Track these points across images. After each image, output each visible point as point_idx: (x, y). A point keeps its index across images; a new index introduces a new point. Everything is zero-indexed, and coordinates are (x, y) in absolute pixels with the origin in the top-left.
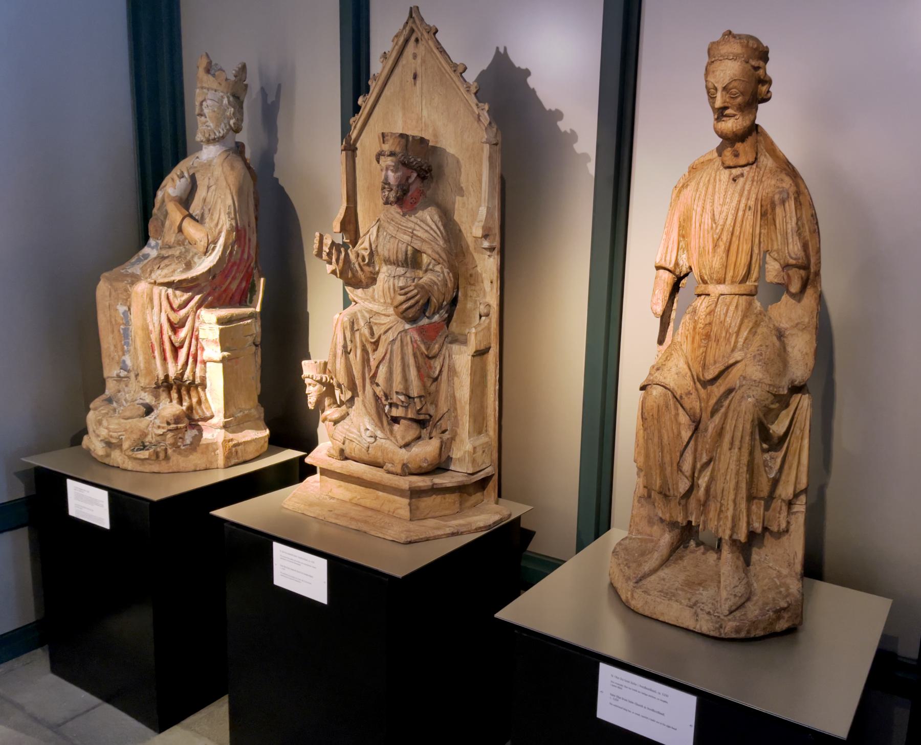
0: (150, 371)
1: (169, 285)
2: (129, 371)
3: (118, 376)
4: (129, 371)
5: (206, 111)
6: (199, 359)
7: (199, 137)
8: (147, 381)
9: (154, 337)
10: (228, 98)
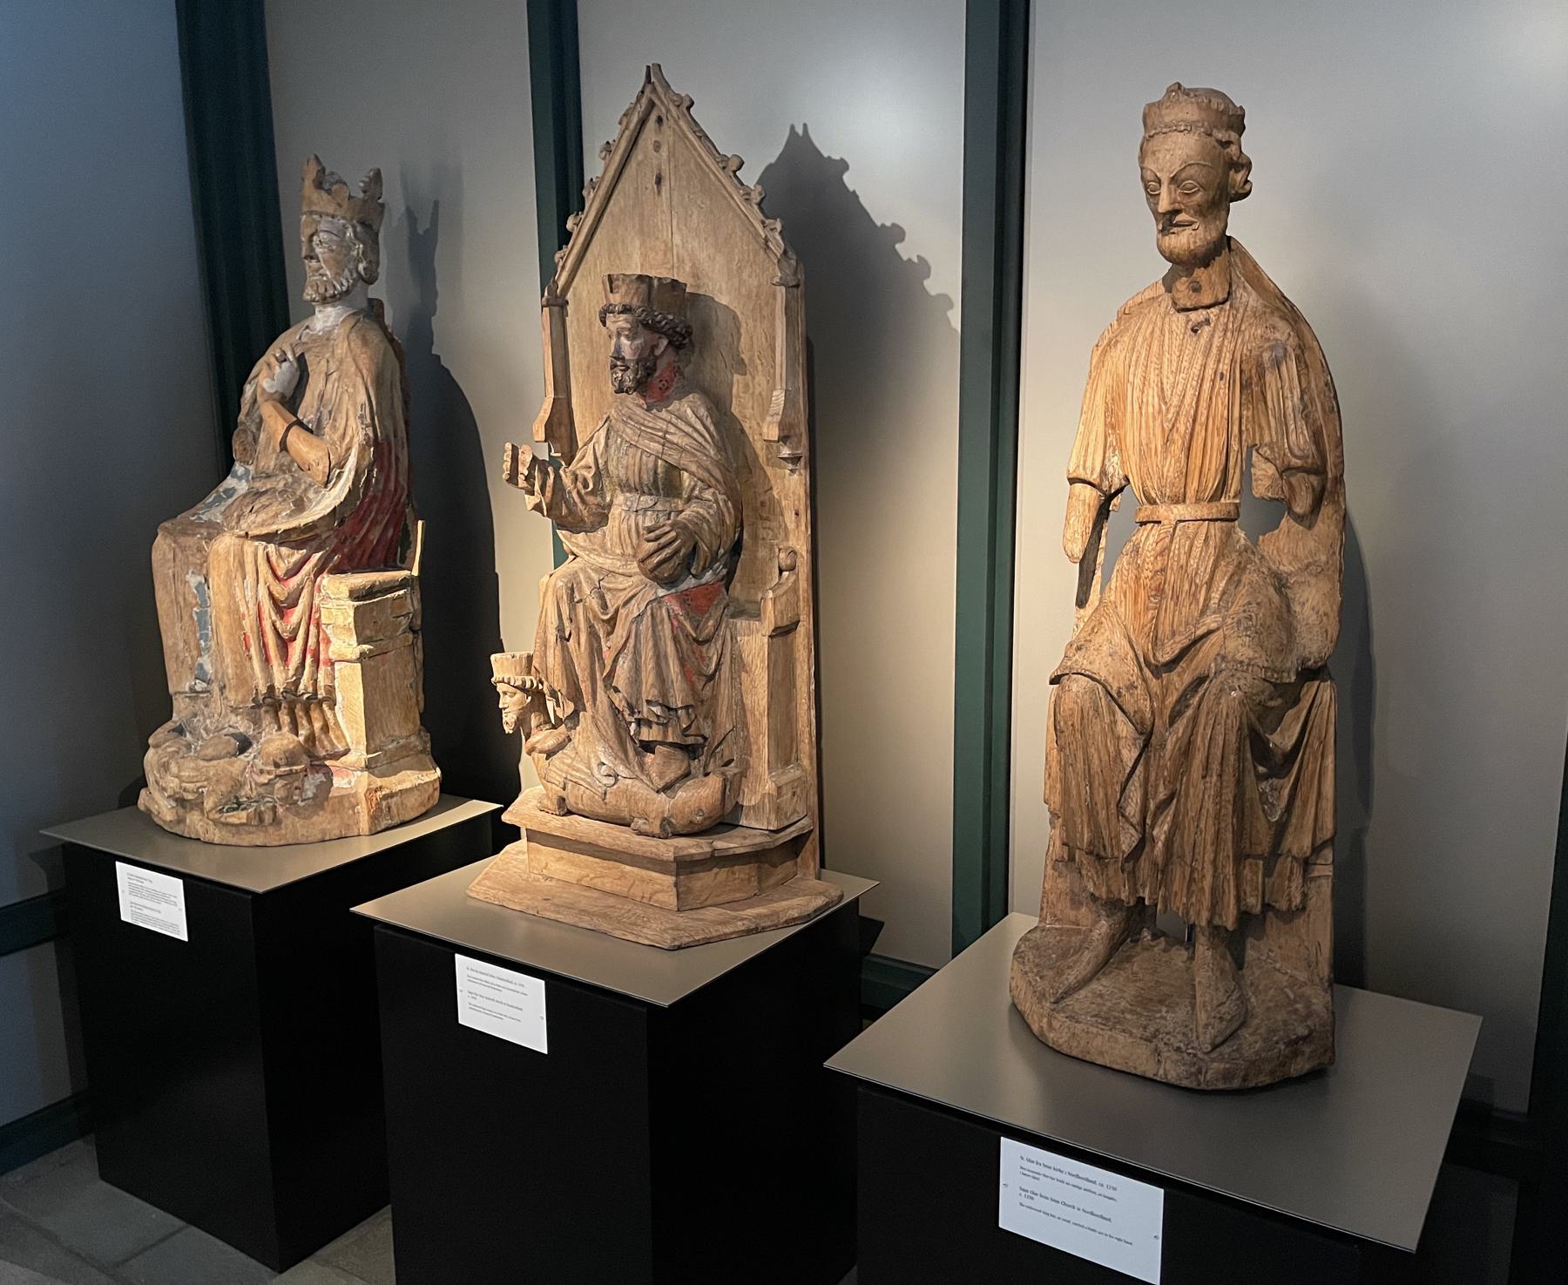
0: (243, 680)
1: (268, 538)
2: (209, 682)
3: (192, 690)
4: (209, 682)
5: (318, 250)
6: (322, 657)
7: (309, 294)
8: (240, 697)
9: (248, 624)
10: (354, 227)
